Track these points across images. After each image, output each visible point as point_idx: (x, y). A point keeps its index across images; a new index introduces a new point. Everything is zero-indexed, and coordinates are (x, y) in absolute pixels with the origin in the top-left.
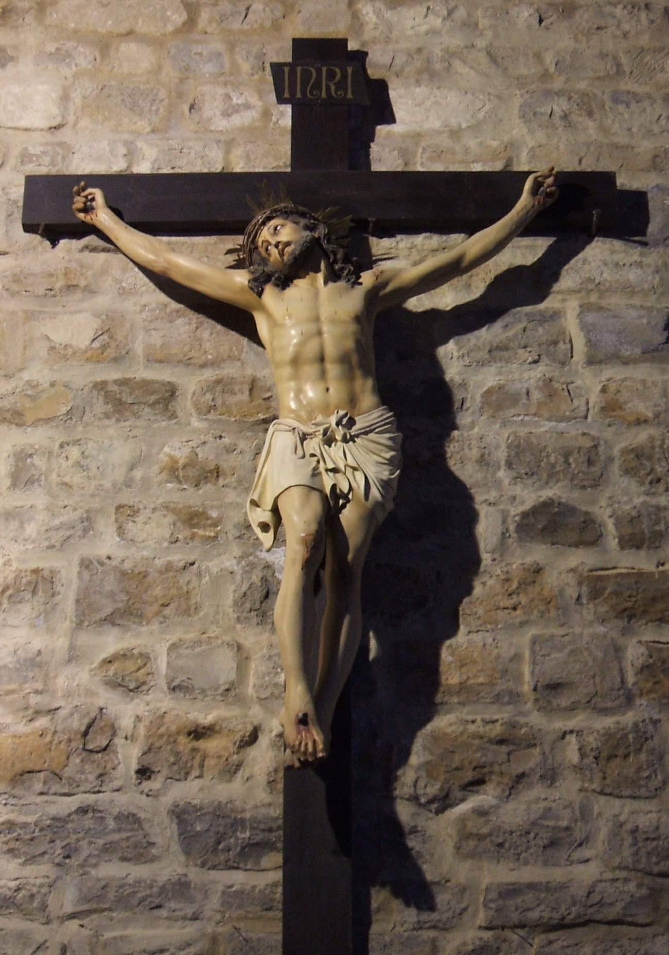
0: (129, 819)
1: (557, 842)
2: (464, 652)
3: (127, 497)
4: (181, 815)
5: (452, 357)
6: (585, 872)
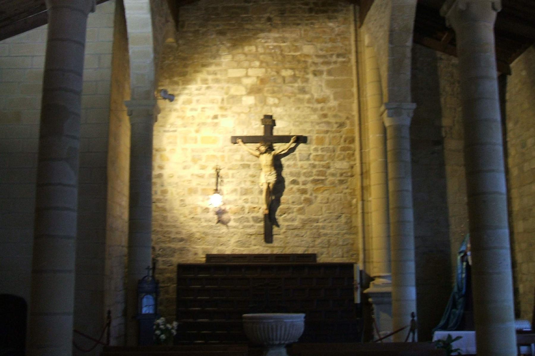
0: (247, 218)
1: (293, 220)
2: (284, 198)
3: (245, 179)
4: (253, 217)
5: (283, 160)
6: (296, 223)
